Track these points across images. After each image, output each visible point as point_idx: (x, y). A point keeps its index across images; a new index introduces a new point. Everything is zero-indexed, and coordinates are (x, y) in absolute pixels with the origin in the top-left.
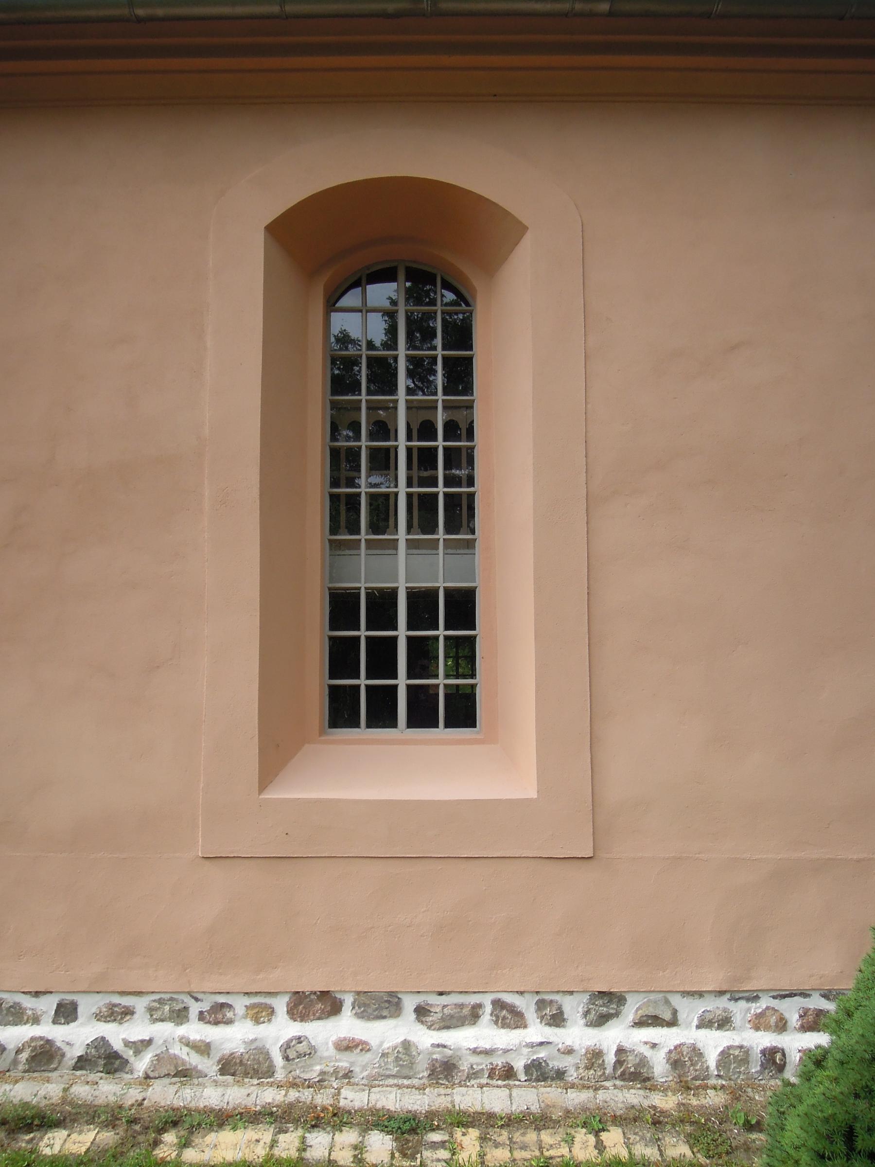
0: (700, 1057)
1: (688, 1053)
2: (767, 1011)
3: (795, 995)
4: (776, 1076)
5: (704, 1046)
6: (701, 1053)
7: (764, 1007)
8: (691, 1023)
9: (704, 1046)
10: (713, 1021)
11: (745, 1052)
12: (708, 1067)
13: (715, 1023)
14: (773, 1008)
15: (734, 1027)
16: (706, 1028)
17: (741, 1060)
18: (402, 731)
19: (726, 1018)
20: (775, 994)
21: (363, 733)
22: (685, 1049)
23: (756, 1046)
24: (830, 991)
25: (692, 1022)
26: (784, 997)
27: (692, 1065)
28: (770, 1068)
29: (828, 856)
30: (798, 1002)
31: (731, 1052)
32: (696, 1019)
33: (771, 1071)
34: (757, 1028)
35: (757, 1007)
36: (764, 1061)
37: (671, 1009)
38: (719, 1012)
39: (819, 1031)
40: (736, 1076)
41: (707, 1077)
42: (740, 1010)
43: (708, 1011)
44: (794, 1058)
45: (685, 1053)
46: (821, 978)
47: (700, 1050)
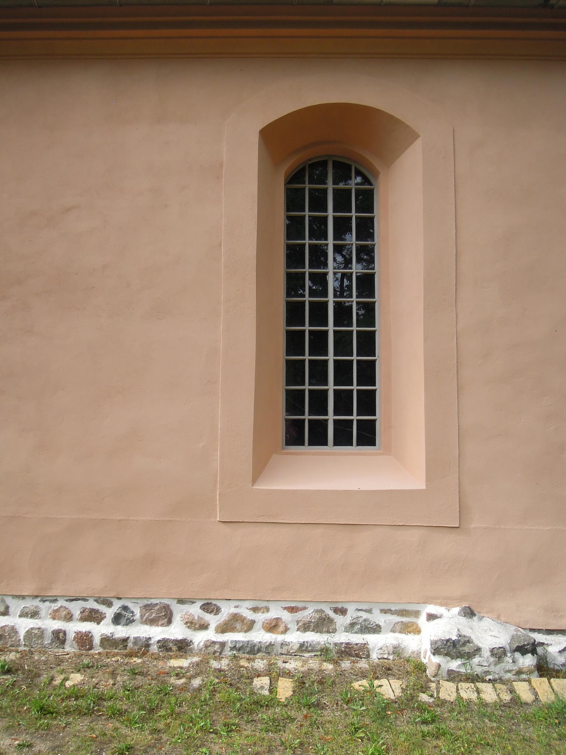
0: (15, 634)
1: (8, 631)
2: (61, 609)
3: (79, 600)
4: (59, 647)
5: (19, 628)
6: (17, 632)
7: (59, 606)
8: (16, 614)
9: (19, 628)
10: (29, 613)
11: (41, 632)
12: (20, 640)
13: (29, 614)
14: (65, 607)
15: (40, 617)
16: (24, 617)
17: (39, 636)
18: (330, 448)
19: (36, 611)
20: (67, 599)
21: (307, 449)
22: (7, 629)
23: (49, 628)
24: (100, 598)
25: (17, 613)
26: (72, 600)
27: (10, 638)
28: (56, 642)
29: (101, 518)
30: (81, 604)
31: (33, 631)
32: (19, 611)
33: (57, 644)
34: (54, 618)
35: (55, 606)
36: (53, 638)
37: (5, 605)
38: (32, 608)
39: (91, 622)
40: (35, 646)
41: (19, 645)
42: (45, 608)
43: (27, 607)
44: (71, 637)
45: (6, 631)
46: (93, 590)
47: (16, 629)
